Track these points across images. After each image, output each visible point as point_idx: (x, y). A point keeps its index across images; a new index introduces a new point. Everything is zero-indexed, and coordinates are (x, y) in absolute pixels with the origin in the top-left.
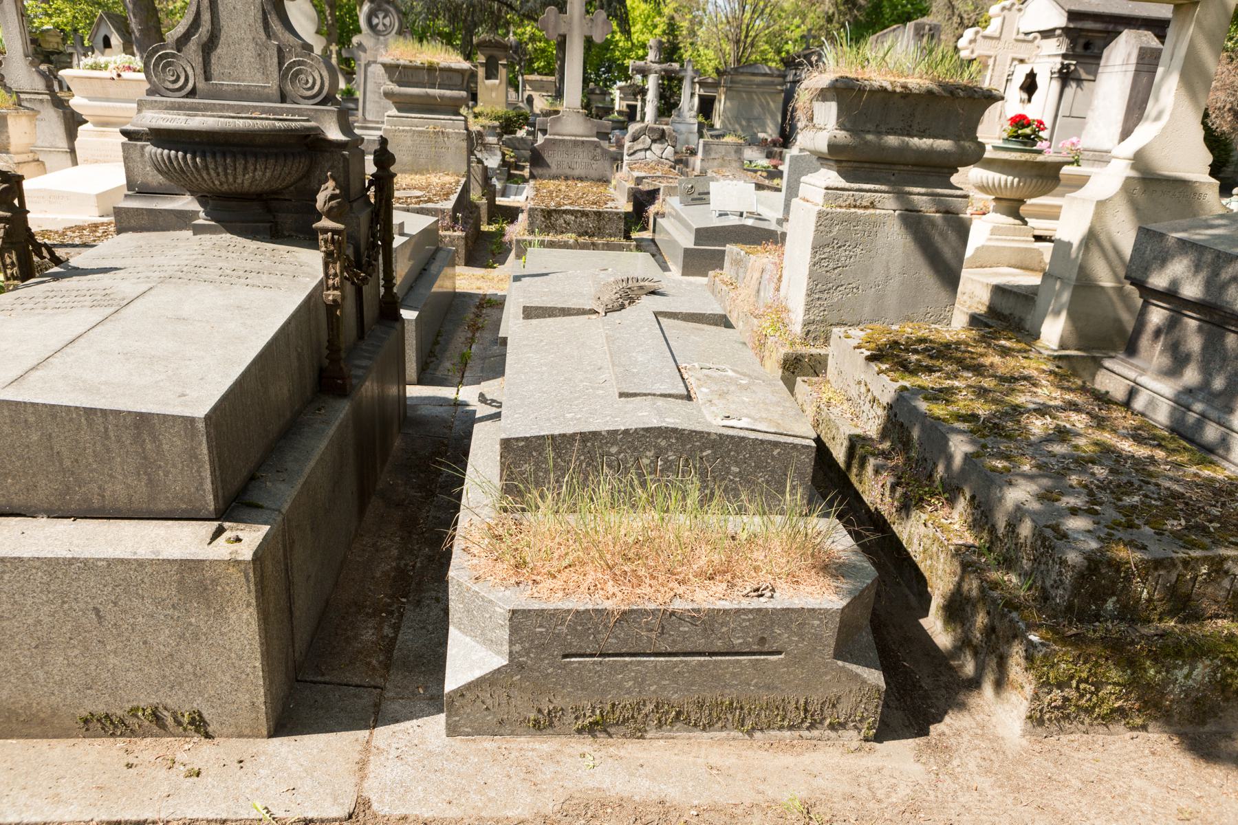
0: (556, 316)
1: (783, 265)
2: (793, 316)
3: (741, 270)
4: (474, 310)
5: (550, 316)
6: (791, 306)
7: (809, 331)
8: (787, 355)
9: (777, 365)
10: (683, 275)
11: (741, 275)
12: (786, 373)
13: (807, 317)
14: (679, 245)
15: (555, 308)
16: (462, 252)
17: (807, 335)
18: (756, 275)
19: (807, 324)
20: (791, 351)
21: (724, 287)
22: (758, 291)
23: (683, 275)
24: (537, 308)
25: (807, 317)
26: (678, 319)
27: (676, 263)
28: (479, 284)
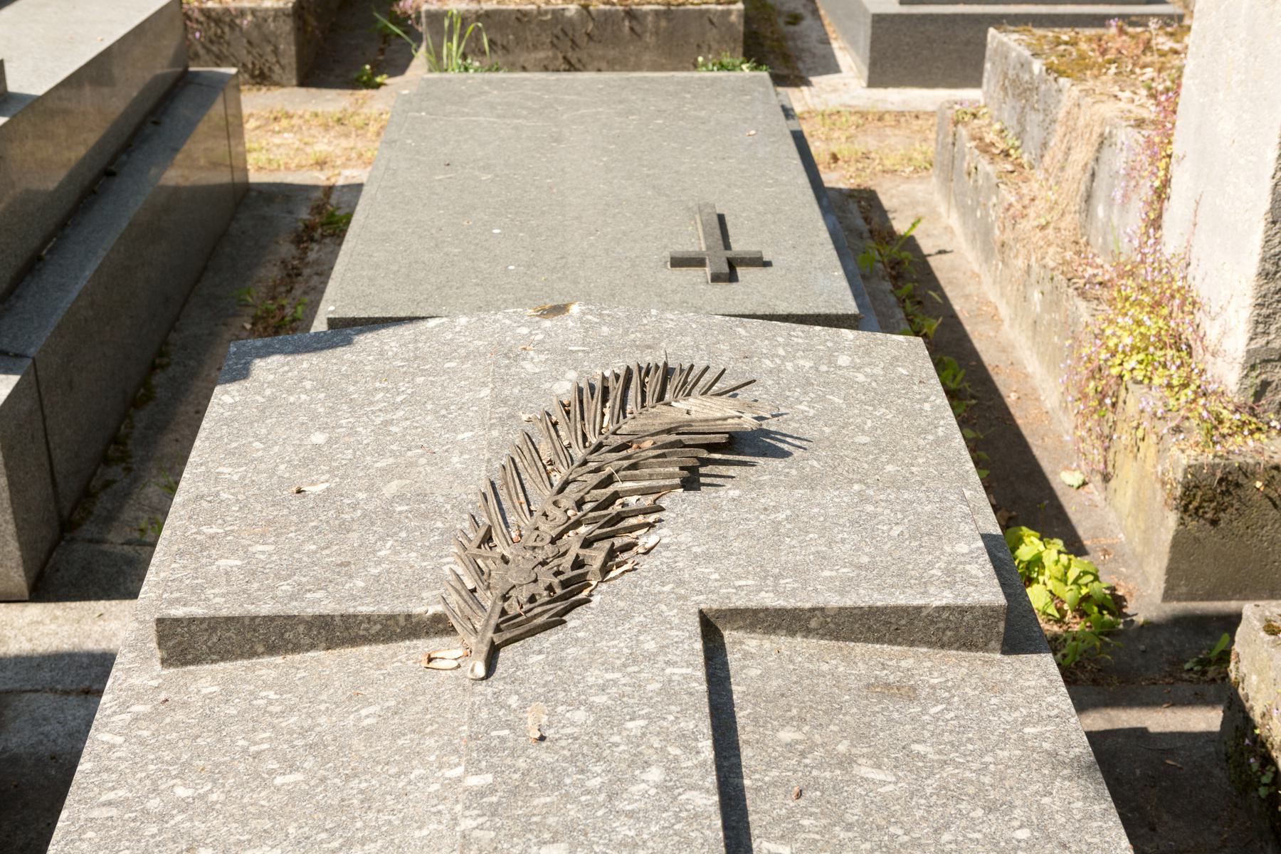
0: (297, 648)
1: (1176, 149)
2: (1212, 331)
3: (1034, 118)
4: (286, 249)
5: (272, 650)
6: (1201, 289)
7: (1265, 385)
8: (1193, 470)
9: (1160, 496)
10: (873, 82)
11: (1034, 132)
12: (1192, 524)
13: (1261, 341)
14: (866, 10)
15: (290, 621)
16: (289, 49)
17: (1258, 395)
18: (1082, 154)
19: (1256, 362)
20: (1208, 458)
21: (984, 165)
22: (1088, 198)
23: (873, 82)
24: (214, 624)
25: (1261, 341)
26: (808, 632)
27: (853, 43)
28: (323, 145)
